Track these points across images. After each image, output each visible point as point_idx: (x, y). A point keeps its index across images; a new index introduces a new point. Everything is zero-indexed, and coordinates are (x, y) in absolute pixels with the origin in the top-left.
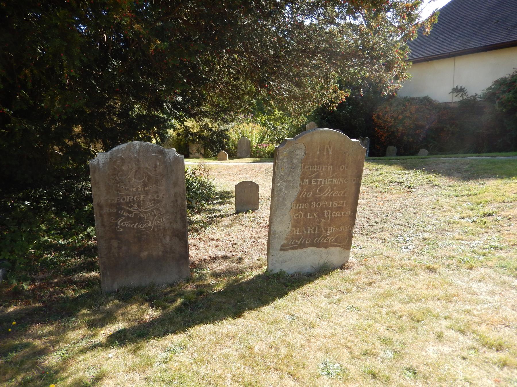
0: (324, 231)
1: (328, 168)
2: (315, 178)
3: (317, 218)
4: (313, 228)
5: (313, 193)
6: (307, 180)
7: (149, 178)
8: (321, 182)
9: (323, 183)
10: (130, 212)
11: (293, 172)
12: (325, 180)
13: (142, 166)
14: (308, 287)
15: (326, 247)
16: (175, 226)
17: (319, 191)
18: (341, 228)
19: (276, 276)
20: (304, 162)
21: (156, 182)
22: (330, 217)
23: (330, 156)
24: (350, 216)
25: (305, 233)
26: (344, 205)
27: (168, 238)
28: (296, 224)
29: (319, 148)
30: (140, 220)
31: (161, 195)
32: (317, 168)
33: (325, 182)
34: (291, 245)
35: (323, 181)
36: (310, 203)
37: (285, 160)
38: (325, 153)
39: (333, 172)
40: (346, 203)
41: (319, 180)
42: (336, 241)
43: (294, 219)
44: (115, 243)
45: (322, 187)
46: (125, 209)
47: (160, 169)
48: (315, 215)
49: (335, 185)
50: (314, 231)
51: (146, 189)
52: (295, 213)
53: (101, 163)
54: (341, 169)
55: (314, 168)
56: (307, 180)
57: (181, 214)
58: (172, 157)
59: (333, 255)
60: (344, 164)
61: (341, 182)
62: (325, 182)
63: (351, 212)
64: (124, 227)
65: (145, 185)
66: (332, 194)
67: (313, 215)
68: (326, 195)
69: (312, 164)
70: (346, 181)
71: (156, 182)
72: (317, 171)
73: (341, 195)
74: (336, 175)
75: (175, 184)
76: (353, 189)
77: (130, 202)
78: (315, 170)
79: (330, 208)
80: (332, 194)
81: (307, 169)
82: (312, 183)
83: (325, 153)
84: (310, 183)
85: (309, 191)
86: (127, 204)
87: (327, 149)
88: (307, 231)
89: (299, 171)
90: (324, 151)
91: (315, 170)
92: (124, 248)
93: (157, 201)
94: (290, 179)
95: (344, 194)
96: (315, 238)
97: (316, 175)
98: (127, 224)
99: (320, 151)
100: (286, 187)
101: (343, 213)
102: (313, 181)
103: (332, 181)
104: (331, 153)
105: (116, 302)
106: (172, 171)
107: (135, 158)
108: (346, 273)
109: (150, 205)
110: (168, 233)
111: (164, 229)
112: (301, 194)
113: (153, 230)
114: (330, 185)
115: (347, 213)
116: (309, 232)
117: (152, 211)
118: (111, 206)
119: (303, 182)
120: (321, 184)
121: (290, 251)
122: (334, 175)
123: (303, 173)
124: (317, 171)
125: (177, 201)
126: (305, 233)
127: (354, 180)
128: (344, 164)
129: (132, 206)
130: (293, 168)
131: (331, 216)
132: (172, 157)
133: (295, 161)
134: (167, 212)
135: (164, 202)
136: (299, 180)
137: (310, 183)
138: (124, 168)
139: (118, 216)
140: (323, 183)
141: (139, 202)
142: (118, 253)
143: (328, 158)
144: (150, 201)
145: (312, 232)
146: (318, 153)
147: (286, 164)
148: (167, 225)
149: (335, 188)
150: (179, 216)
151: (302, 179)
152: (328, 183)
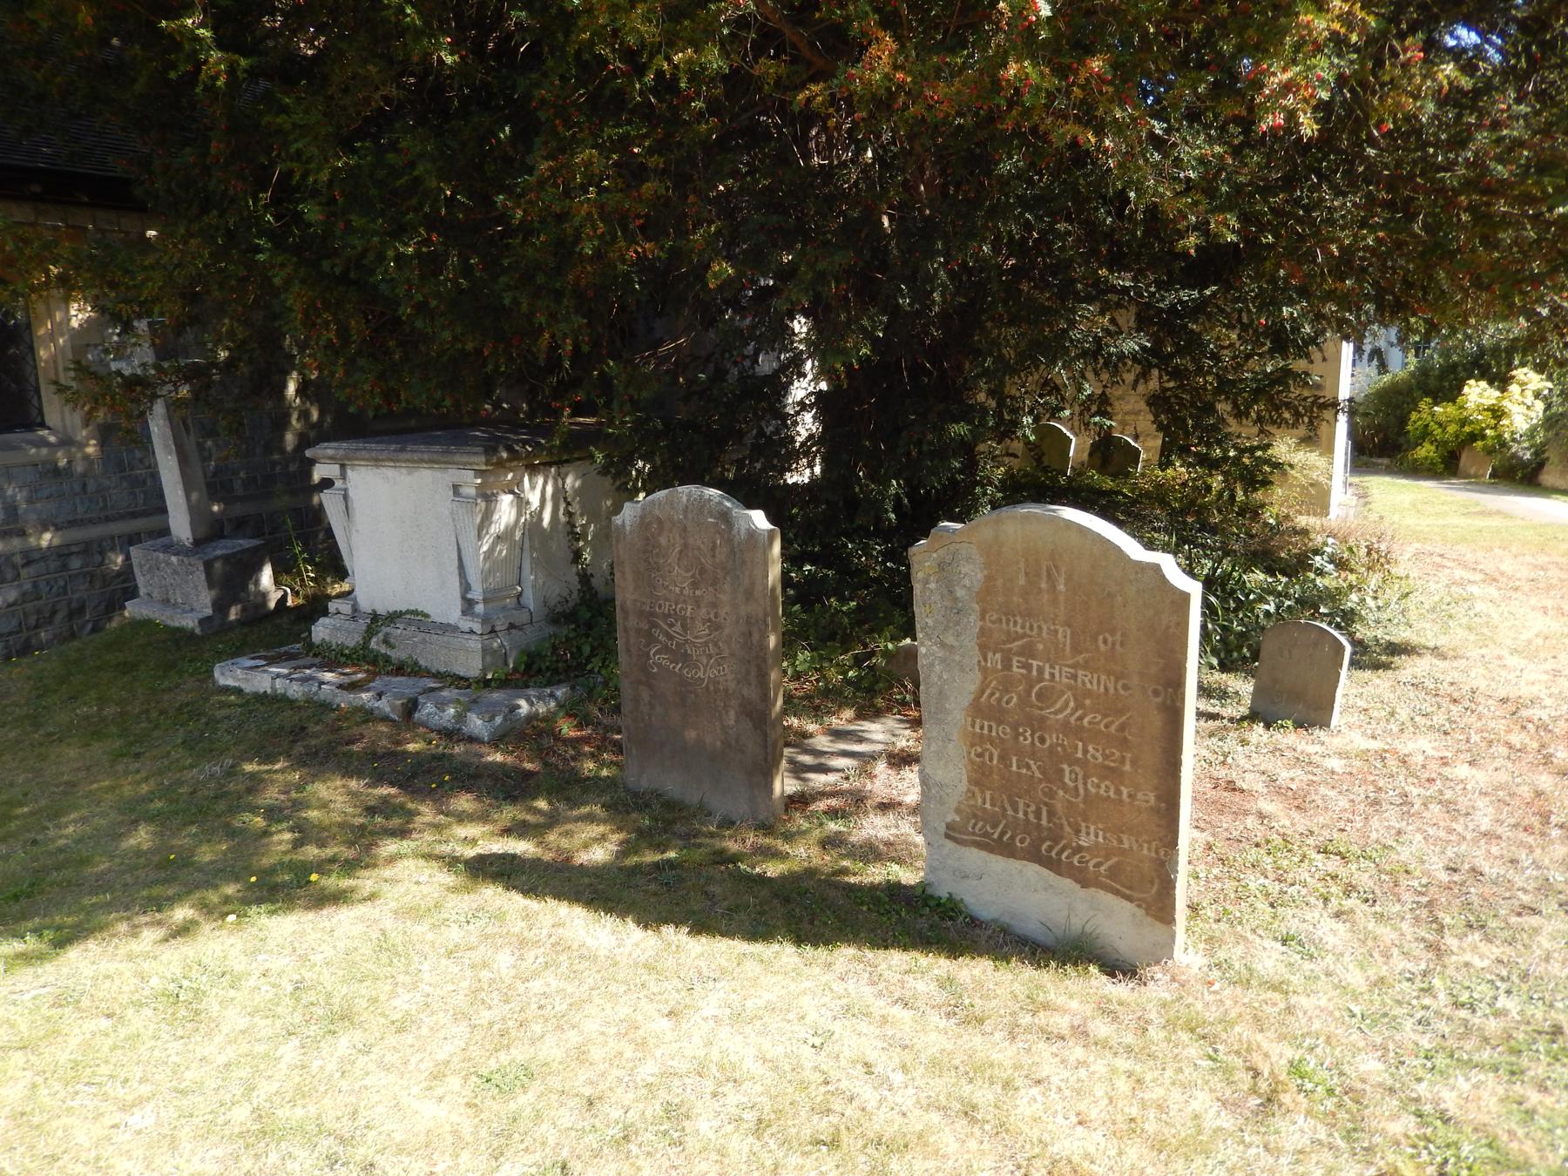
0: (1067, 829)
1: (1056, 631)
2: (1019, 654)
3: (1040, 781)
4: (1033, 808)
5: (1019, 697)
6: (998, 656)
7: (703, 571)
8: (1040, 670)
9: (1047, 676)
10: (671, 638)
11: (957, 623)
12: (1052, 667)
13: (691, 541)
14: (974, 971)
15: (1084, 883)
16: (745, 692)
17: (1039, 696)
18: (1124, 837)
19: (932, 903)
20: (985, 594)
21: (715, 583)
22: (1082, 791)
23: (1061, 598)
24: (1155, 810)
25: (1010, 812)
26: (1127, 767)
27: (732, 714)
28: (980, 777)
29: (1022, 565)
30: (685, 658)
31: (722, 613)
32: (1023, 627)
33: (1052, 675)
34: (974, 834)
35: (1047, 670)
36: (1015, 728)
37: (932, 586)
38: (1044, 585)
39: (1076, 650)
40: (1134, 762)
41: (1035, 663)
42: (1114, 873)
43: (972, 762)
44: (645, 695)
45: (1045, 688)
46: (661, 629)
47: (722, 554)
48: (1034, 767)
49: (1089, 694)
50: (1038, 817)
51: (698, 593)
52: (972, 745)
53: (628, 523)
54: (1102, 647)
55: (1015, 623)
56: (998, 656)
57: (758, 666)
58: (743, 531)
59: (1114, 919)
60: (1113, 632)
61: (1106, 689)
62: (1052, 675)
63: (1158, 798)
64: (659, 666)
65: (695, 585)
66: (1081, 718)
67: (1028, 767)
68: (1060, 716)
69: (1009, 613)
70: (1125, 687)
71: (715, 583)
72: (1024, 636)
73: (1113, 728)
74: (1086, 662)
75: (749, 595)
76: (1156, 721)
77: (669, 615)
78: (1018, 629)
79: (1077, 762)
80: (1081, 718)
81: (993, 622)
82: (1015, 669)
83: (1044, 585)
84: (1007, 665)
85: (1007, 691)
86: (666, 616)
87: (1049, 575)
88: (1016, 811)
89: (973, 622)
90: (1038, 575)
91: (1018, 629)
92: (659, 710)
93: (715, 626)
94: (950, 640)
95: (1122, 728)
96: (1043, 841)
97: (1023, 647)
98: (663, 659)
99: (1027, 574)
100: (943, 660)
101: (1125, 791)
102: (1015, 664)
103: (1074, 677)
104: (1061, 587)
105: (597, 809)
106: (744, 562)
107: (680, 521)
108: (1120, 990)
109: (702, 630)
110: (734, 702)
111: (726, 690)
112: (983, 692)
113: (707, 687)
114: (1070, 688)
115: (1140, 796)
116: (1021, 815)
117: (706, 644)
118: (641, 614)
119: (986, 660)
120: (1041, 680)
121: (974, 851)
122: (1080, 658)
123: (982, 632)
124: (1024, 636)
125: (750, 634)
126: (1010, 812)
127: (1156, 693)
128: (1113, 632)
129: (672, 625)
130: (956, 611)
131: (1086, 789)
132: (743, 531)
133: (960, 593)
134: (732, 655)
135: (727, 631)
136: (976, 655)
137: (1007, 665)
138: (663, 541)
139: (651, 640)
140: (1047, 676)
141: (684, 619)
142: (650, 716)
143: (1055, 602)
144: (704, 622)
145: (1031, 817)
146: (1022, 581)
147: (936, 597)
148: (732, 685)
149: (1088, 702)
150: (754, 672)
151: (983, 649)
152: (1065, 680)
